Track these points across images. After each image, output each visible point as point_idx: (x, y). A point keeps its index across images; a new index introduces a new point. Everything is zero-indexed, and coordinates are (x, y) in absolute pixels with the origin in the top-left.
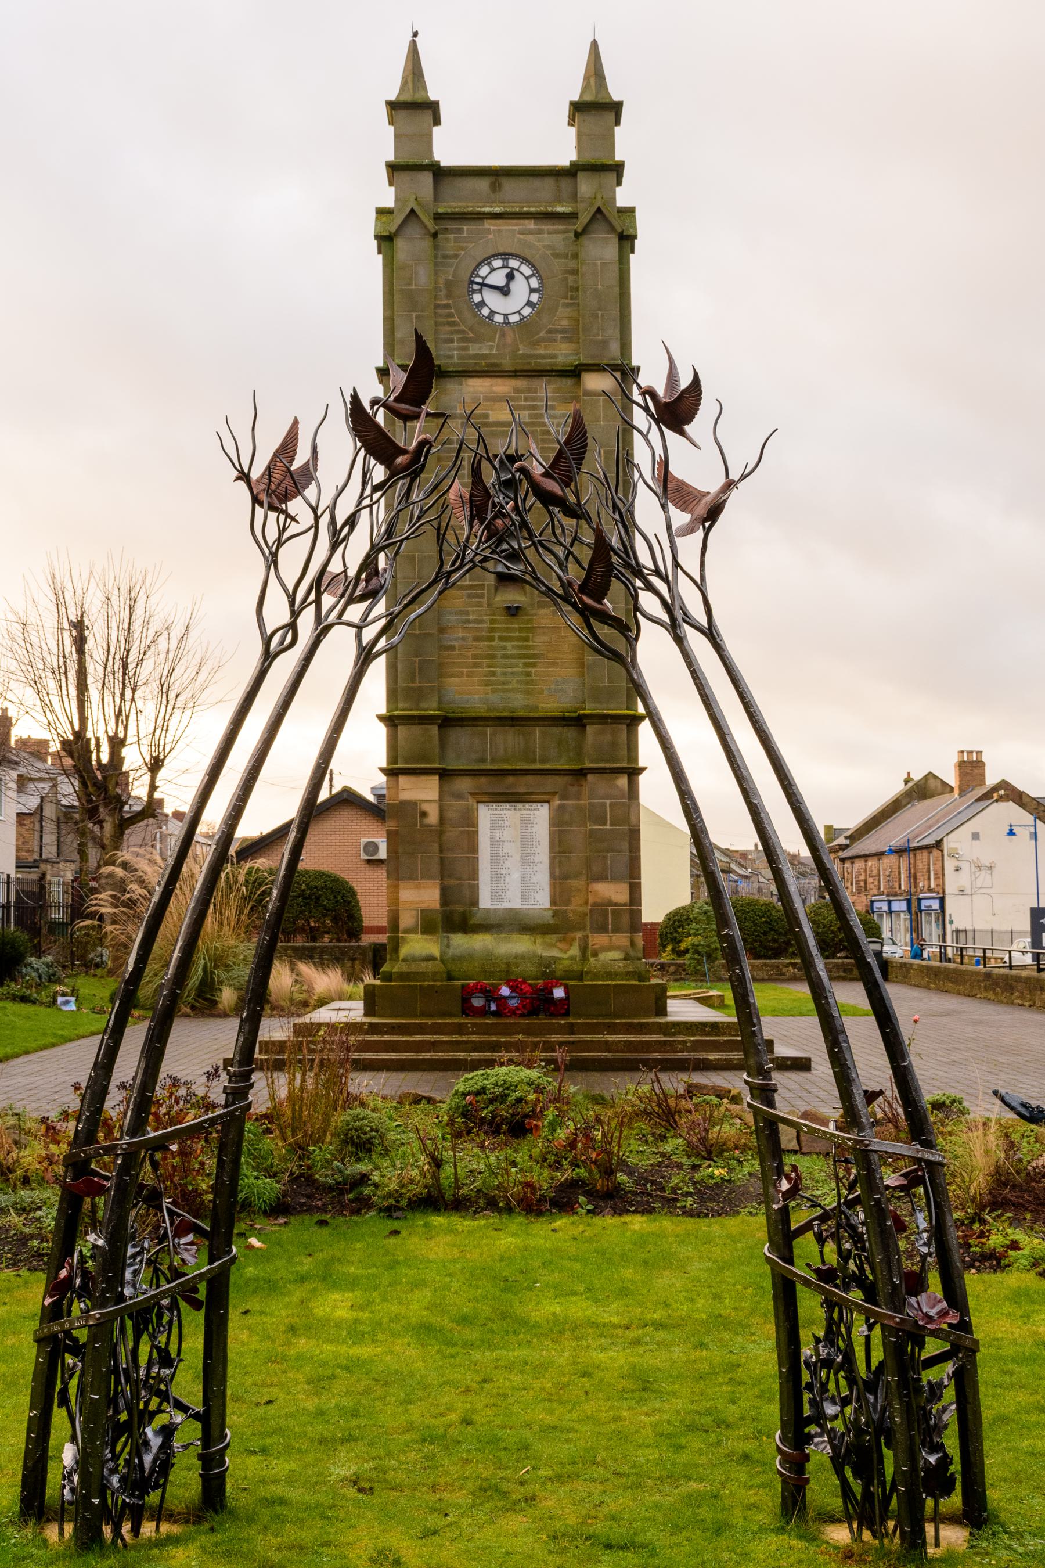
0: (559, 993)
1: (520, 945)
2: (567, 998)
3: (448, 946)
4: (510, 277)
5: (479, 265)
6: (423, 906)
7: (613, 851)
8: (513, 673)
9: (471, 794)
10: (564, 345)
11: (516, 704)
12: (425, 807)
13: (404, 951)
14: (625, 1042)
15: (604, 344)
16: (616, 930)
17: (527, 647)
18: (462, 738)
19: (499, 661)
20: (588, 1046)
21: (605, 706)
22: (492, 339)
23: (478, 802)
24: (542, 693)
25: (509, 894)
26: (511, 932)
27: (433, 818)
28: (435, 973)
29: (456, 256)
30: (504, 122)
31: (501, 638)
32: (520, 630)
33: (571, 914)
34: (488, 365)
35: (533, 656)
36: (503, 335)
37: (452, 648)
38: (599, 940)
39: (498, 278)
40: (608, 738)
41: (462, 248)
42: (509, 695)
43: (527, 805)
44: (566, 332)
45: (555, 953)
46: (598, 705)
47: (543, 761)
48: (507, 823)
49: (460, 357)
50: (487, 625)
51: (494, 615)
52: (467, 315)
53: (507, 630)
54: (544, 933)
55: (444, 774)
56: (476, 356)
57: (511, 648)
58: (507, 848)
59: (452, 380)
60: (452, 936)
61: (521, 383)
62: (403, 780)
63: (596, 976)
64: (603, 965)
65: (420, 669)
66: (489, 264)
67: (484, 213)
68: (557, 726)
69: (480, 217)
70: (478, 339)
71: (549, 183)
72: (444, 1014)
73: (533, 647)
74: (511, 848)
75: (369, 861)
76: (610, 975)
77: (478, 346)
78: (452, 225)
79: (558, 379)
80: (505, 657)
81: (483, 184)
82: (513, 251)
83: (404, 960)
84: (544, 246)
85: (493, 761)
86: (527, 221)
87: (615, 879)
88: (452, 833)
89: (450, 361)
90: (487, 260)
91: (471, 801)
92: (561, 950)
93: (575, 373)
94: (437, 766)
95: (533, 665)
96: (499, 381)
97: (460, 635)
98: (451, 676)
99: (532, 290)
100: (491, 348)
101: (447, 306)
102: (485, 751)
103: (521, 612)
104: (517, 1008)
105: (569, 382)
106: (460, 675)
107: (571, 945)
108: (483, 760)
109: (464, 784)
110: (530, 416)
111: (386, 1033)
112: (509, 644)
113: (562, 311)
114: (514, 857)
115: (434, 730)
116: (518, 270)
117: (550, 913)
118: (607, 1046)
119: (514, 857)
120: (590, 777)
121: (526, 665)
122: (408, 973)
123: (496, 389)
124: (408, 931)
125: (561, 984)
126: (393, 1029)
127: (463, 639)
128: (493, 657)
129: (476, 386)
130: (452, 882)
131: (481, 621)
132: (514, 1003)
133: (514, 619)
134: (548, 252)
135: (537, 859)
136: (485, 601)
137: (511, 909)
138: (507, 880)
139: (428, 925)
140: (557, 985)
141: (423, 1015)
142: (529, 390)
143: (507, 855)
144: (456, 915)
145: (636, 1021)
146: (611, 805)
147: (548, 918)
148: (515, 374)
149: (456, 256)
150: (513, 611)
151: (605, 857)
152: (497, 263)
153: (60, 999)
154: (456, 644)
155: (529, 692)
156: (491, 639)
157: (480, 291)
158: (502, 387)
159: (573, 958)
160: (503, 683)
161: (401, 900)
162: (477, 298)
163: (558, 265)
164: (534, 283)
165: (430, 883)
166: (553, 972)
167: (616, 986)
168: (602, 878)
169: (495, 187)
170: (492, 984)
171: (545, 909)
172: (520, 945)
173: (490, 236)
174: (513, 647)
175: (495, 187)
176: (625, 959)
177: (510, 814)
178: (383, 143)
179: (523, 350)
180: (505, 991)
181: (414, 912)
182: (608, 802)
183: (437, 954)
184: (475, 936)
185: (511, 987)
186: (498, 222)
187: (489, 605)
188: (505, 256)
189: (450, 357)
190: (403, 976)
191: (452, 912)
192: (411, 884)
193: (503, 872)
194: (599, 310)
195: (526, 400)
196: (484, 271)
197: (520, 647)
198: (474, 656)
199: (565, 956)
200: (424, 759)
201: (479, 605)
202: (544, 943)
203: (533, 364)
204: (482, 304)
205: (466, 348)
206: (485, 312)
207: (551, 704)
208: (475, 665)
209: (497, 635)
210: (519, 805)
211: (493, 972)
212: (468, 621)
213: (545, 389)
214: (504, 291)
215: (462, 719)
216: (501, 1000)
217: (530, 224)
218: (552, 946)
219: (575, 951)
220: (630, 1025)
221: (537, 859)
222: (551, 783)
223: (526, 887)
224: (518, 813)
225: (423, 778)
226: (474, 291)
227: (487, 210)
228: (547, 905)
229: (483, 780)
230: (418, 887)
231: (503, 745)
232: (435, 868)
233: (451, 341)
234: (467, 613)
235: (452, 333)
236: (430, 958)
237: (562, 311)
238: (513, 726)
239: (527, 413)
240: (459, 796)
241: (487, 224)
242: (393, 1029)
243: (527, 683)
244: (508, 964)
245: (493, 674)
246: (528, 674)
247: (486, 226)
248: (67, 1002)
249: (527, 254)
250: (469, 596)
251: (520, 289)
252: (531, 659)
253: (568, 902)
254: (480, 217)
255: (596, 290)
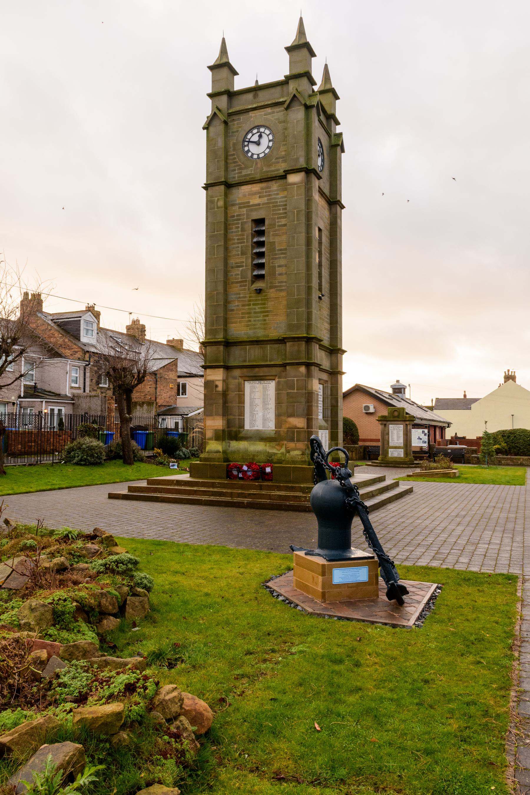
0: (268, 470)
1: (259, 447)
2: (272, 472)
3: (229, 446)
4: (260, 136)
5: (247, 134)
6: (216, 428)
7: (298, 402)
8: (258, 320)
9: (240, 377)
10: (283, 164)
11: (260, 335)
12: (217, 383)
13: (208, 448)
14: (278, 495)
15: (297, 159)
16: (298, 440)
17: (264, 308)
18: (236, 351)
19: (253, 315)
20: (261, 496)
21: (294, 333)
22: (252, 167)
23: (244, 381)
24: (270, 328)
25: (257, 423)
26: (256, 440)
27: (220, 389)
28: (219, 458)
29: (237, 131)
30: (261, 65)
31: (254, 304)
32: (262, 300)
33: (282, 433)
34: (250, 178)
35: (267, 312)
36: (257, 164)
37: (233, 310)
38: (292, 445)
39: (255, 138)
40: (296, 348)
41: (240, 127)
42: (257, 330)
43: (266, 382)
44: (284, 158)
45: (275, 451)
46: (292, 333)
47: (270, 361)
48: (257, 390)
49: (238, 177)
50: (248, 298)
51: (250, 294)
52: (242, 157)
53: (256, 300)
54: (270, 442)
55: (227, 368)
56: (245, 175)
57: (258, 309)
58: (257, 401)
59: (235, 188)
60: (231, 442)
61: (264, 185)
62: (208, 371)
63: (288, 463)
64: (291, 457)
65: (216, 320)
66: (252, 132)
67: (248, 109)
68: (277, 344)
69: (247, 111)
70: (246, 168)
71: (279, 89)
72: (219, 478)
73: (267, 308)
74: (258, 401)
75: (367, 413)
76: (294, 462)
77: (245, 170)
78: (235, 117)
79: (280, 180)
80: (255, 313)
81: (250, 96)
82: (261, 124)
83: (208, 452)
84: (275, 119)
85: (249, 361)
86: (267, 109)
87: (298, 416)
88: (232, 395)
89: (234, 180)
90: (250, 131)
91: (241, 380)
92: (278, 450)
93: (284, 177)
94: (222, 364)
95: (267, 316)
96: (254, 185)
97: (237, 304)
98: (232, 323)
99: (270, 141)
100: (251, 170)
101: (234, 155)
102: (246, 357)
103: (262, 292)
104: (250, 476)
105: (281, 182)
106: (236, 323)
107: (282, 447)
108: (245, 361)
109: (237, 372)
110: (268, 200)
111: (183, 485)
112: (257, 307)
113: (282, 148)
114: (261, 405)
115: (221, 348)
116: (264, 133)
117: (274, 432)
118: (270, 497)
119: (261, 405)
120: (288, 367)
121: (264, 316)
122: (208, 458)
123: (253, 189)
124: (210, 439)
125: (270, 466)
126: (203, 484)
127: (238, 306)
128: (250, 313)
129: (245, 189)
130: (231, 417)
131: (245, 297)
132: (250, 474)
133: (260, 295)
134: (277, 122)
135: (270, 406)
136: (247, 287)
137: (258, 430)
138: (257, 416)
139: (220, 436)
140: (268, 466)
141: (213, 478)
142: (268, 187)
143: (257, 405)
144: (233, 432)
145: (290, 485)
146: (297, 380)
147: (273, 434)
148: (261, 181)
149: (237, 131)
150: (259, 291)
151: (294, 406)
152: (255, 131)
153: (171, 464)
154: (235, 308)
155: (265, 329)
156: (249, 305)
157: (248, 145)
158: (255, 188)
159: (282, 453)
160: (254, 325)
161: (207, 425)
162: (246, 149)
163: (280, 126)
164: (271, 137)
165: (218, 417)
166: (272, 460)
167: (293, 467)
168: (292, 415)
169: (255, 96)
170: (240, 465)
171: (273, 430)
172: (259, 447)
173: (252, 119)
174: (259, 308)
175: (255, 96)
176: (302, 455)
177: (258, 386)
178: (206, 83)
179: (265, 169)
180: (245, 468)
181: (212, 431)
182: (295, 379)
183: (221, 450)
184: (241, 442)
185: (247, 466)
186: (255, 112)
187: (249, 289)
188: (258, 127)
189: (234, 178)
190: (206, 459)
191: (231, 431)
192: (211, 418)
193: (255, 412)
194: (295, 143)
195: (266, 192)
196: (250, 135)
197: (261, 308)
198: (243, 313)
199: (279, 452)
200: (217, 361)
201: (245, 290)
202: (270, 446)
203: (270, 175)
204: (249, 151)
205: (241, 173)
206: (250, 154)
207: (274, 334)
208: (242, 318)
209: (252, 303)
210: (262, 382)
211: (247, 459)
212: (240, 298)
213: (275, 186)
214: (258, 143)
215: (235, 343)
216: (244, 472)
217: (269, 110)
218: (273, 447)
219: (283, 450)
220: (287, 487)
221: (270, 406)
222: (274, 371)
223: (265, 420)
224: (262, 385)
225: (217, 370)
226: (245, 146)
227: (250, 107)
228: (274, 428)
229: (245, 370)
230: (213, 419)
231: (253, 354)
232: (221, 411)
233: (235, 170)
234: (239, 294)
235: (235, 166)
236: (218, 452)
237: (282, 148)
238: (258, 345)
239: (266, 198)
240: (235, 378)
241: (251, 114)
242: (203, 484)
243: (264, 324)
244: (254, 455)
245: (250, 321)
246: (265, 320)
247: (250, 115)
248: (173, 466)
249: (267, 125)
250: (241, 286)
251: (265, 141)
252: (266, 313)
253: (281, 427)
254: (247, 111)
255: (294, 134)
